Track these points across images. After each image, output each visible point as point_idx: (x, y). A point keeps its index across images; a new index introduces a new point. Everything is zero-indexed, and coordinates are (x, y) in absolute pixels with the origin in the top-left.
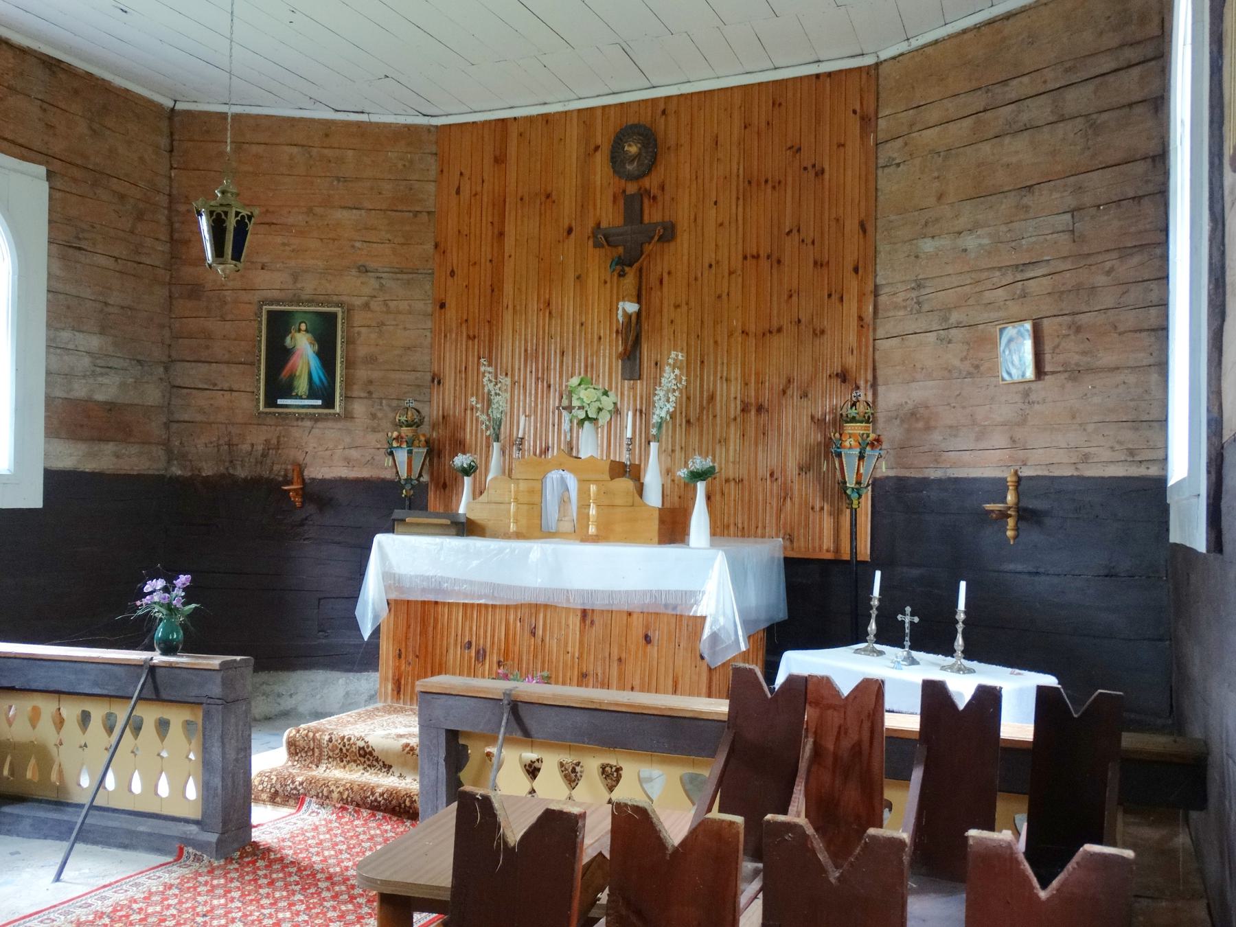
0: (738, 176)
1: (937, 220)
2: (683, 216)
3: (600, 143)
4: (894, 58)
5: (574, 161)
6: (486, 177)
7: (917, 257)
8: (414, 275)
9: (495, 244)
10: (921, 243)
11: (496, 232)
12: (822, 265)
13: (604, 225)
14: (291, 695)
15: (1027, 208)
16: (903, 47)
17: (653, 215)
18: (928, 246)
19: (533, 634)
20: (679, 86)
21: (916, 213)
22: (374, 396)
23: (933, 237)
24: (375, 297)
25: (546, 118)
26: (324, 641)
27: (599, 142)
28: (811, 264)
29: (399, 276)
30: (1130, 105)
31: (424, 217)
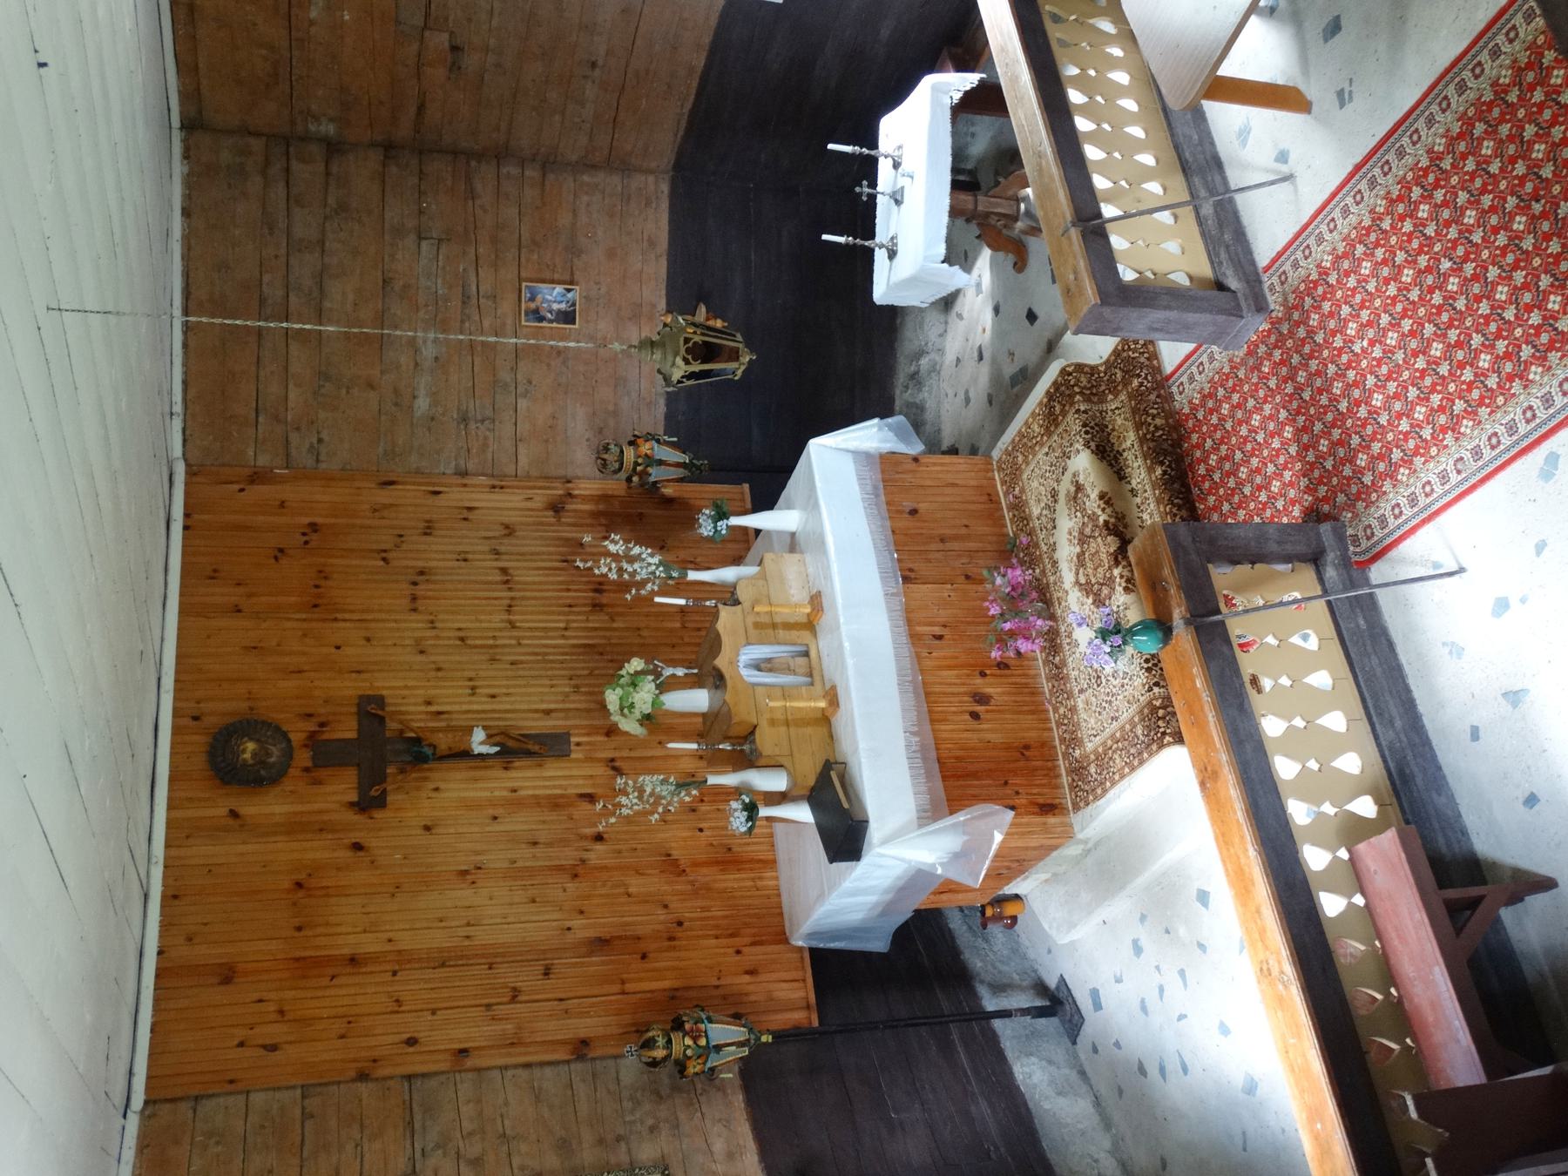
0: (305, 620)
1: (396, 391)
2: (350, 688)
3: (227, 809)
4: (185, 441)
5: (250, 848)
6: (256, 996)
7: (433, 419)
8: (414, 1106)
9: (369, 969)
10: (418, 414)
11: (349, 969)
12: (429, 528)
13: (354, 797)
14: (1096, 1161)
15: (406, 287)
16: (177, 424)
17: (347, 730)
18: (422, 404)
19: (940, 637)
20: (162, 690)
21: (383, 418)
22: (622, 1133)
23: (415, 397)
24: (458, 1153)
25: (171, 898)
26: (1002, 1150)
27: (223, 811)
28: (428, 539)
29: (417, 1126)
30: (328, 174)
31: (313, 1103)
